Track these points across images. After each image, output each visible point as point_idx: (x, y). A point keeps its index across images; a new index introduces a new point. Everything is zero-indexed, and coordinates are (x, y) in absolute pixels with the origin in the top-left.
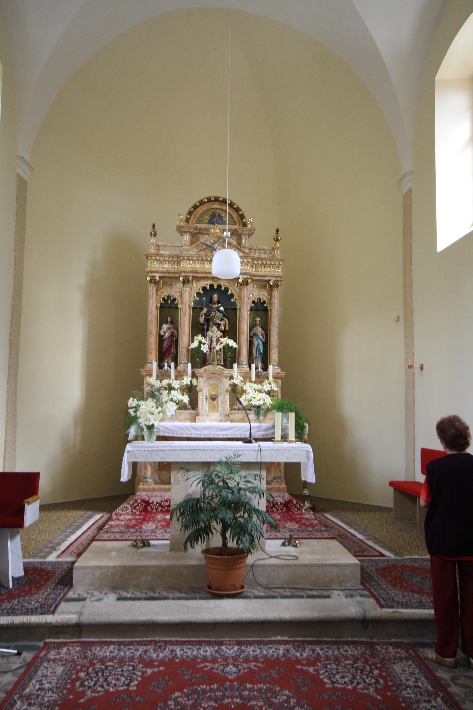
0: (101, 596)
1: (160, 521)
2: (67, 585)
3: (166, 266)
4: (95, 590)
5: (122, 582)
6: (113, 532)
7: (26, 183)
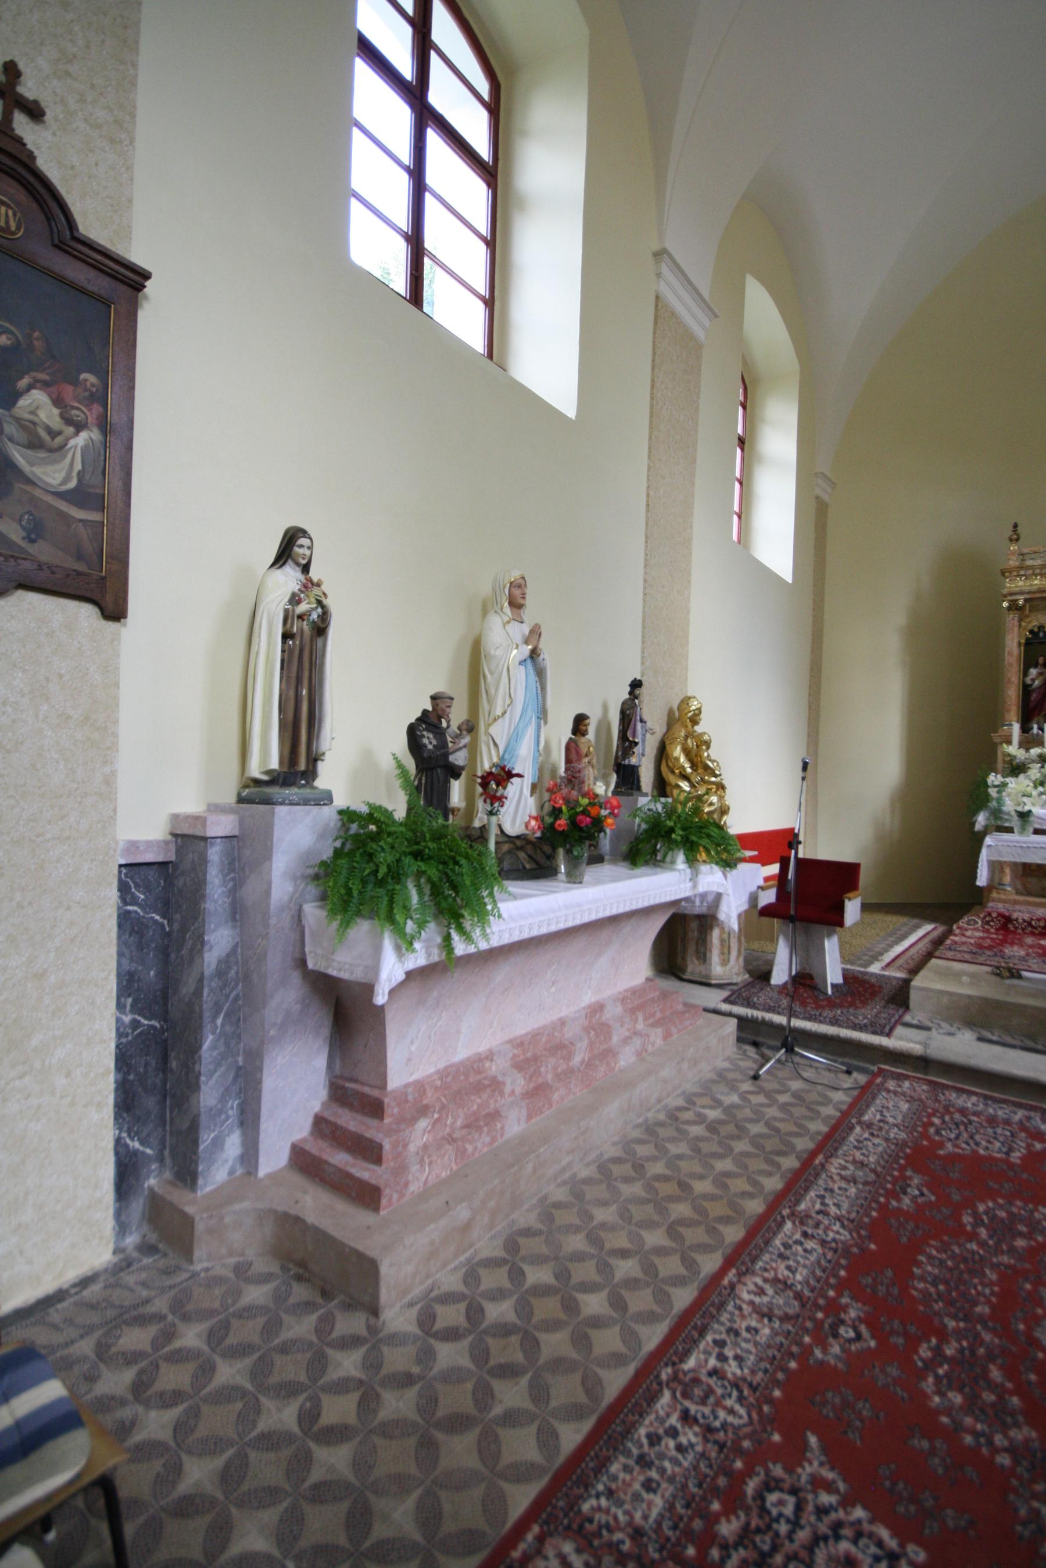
0: (952, 1030)
1: (1032, 947)
2: (901, 1006)
3: (1036, 582)
4: (943, 1020)
5: (981, 1017)
6: (960, 951)
7: (826, 505)
